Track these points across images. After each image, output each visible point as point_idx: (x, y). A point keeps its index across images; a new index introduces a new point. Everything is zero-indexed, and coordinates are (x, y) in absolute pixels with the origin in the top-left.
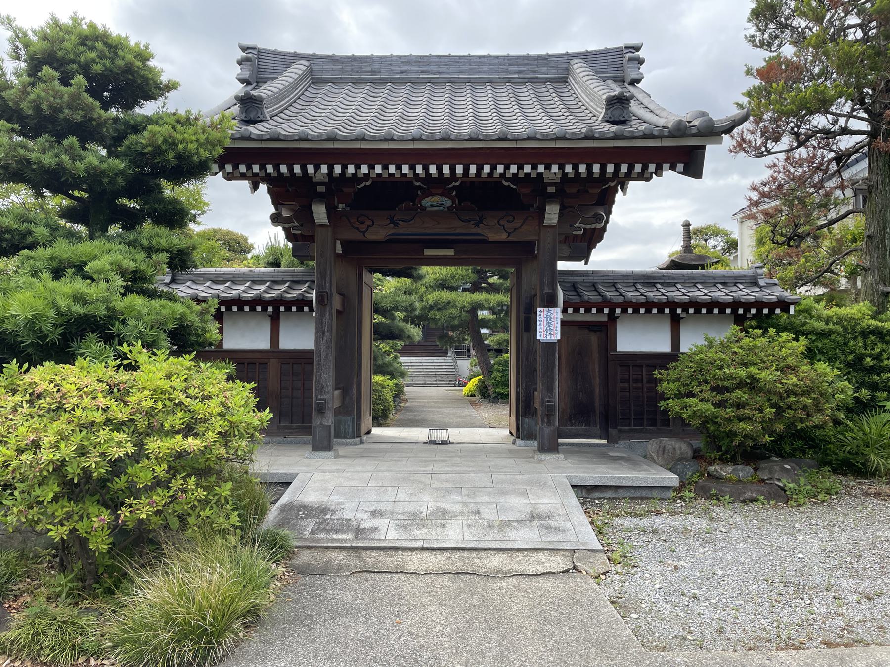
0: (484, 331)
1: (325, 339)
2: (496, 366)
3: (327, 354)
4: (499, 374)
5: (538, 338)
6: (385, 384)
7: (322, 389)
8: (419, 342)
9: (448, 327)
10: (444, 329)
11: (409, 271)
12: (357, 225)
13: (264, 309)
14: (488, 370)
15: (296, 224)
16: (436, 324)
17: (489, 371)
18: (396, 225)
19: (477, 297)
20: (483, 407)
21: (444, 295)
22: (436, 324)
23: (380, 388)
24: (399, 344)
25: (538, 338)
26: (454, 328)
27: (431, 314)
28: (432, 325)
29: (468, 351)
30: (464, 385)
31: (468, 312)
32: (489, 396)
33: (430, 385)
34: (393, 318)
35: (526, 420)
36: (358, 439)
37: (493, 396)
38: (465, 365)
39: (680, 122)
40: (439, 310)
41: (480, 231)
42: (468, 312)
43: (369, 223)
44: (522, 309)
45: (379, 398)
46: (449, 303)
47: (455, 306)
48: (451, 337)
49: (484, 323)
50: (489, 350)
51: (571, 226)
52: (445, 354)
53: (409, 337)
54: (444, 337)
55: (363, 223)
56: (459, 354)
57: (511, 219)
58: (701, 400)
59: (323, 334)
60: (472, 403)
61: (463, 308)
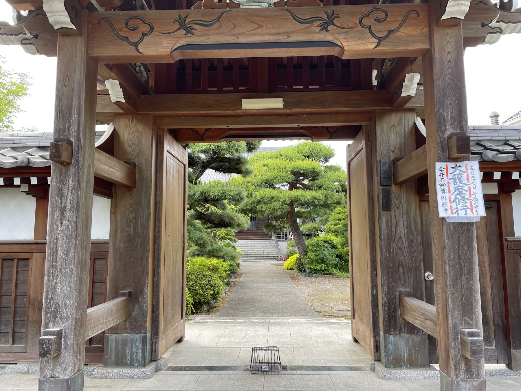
1: (66, 222)
2: (310, 247)
3: (68, 249)
4: (313, 254)
5: (442, 214)
6: (220, 265)
7: (56, 311)
8: (248, 229)
9: (272, 218)
10: (269, 219)
11: (238, 166)
12: (125, 32)
13: (25, 180)
14: (304, 251)
15: (28, 35)
16: (263, 215)
17: (305, 252)
18: (189, 30)
19: (296, 193)
20: (301, 281)
21: (269, 192)
22: (263, 215)
23: (210, 273)
24: (233, 231)
25: (442, 214)
26: (276, 218)
27: (259, 207)
28: (260, 216)
29: (286, 235)
30: (285, 259)
32: (305, 271)
33: (259, 260)
34: (224, 208)
35: (392, 338)
36: (153, 365)
38: (284, 245)
41: (329, 38)
43: (145, 28)
44: (376, 179)
45: (209, 283)
46: (273, 198)
47: (277, 200)
48: (274, 226)
49: (300, 215)
50: (303, 235)
51: (483, 25)
53: (239, 225)
54: (269, 226)
55: (134, 29)
56: (279, 237)
57: (382, 15)
58: (334, 247)
59: (63, 214)
60: (292, 277)
61: (283, 202)
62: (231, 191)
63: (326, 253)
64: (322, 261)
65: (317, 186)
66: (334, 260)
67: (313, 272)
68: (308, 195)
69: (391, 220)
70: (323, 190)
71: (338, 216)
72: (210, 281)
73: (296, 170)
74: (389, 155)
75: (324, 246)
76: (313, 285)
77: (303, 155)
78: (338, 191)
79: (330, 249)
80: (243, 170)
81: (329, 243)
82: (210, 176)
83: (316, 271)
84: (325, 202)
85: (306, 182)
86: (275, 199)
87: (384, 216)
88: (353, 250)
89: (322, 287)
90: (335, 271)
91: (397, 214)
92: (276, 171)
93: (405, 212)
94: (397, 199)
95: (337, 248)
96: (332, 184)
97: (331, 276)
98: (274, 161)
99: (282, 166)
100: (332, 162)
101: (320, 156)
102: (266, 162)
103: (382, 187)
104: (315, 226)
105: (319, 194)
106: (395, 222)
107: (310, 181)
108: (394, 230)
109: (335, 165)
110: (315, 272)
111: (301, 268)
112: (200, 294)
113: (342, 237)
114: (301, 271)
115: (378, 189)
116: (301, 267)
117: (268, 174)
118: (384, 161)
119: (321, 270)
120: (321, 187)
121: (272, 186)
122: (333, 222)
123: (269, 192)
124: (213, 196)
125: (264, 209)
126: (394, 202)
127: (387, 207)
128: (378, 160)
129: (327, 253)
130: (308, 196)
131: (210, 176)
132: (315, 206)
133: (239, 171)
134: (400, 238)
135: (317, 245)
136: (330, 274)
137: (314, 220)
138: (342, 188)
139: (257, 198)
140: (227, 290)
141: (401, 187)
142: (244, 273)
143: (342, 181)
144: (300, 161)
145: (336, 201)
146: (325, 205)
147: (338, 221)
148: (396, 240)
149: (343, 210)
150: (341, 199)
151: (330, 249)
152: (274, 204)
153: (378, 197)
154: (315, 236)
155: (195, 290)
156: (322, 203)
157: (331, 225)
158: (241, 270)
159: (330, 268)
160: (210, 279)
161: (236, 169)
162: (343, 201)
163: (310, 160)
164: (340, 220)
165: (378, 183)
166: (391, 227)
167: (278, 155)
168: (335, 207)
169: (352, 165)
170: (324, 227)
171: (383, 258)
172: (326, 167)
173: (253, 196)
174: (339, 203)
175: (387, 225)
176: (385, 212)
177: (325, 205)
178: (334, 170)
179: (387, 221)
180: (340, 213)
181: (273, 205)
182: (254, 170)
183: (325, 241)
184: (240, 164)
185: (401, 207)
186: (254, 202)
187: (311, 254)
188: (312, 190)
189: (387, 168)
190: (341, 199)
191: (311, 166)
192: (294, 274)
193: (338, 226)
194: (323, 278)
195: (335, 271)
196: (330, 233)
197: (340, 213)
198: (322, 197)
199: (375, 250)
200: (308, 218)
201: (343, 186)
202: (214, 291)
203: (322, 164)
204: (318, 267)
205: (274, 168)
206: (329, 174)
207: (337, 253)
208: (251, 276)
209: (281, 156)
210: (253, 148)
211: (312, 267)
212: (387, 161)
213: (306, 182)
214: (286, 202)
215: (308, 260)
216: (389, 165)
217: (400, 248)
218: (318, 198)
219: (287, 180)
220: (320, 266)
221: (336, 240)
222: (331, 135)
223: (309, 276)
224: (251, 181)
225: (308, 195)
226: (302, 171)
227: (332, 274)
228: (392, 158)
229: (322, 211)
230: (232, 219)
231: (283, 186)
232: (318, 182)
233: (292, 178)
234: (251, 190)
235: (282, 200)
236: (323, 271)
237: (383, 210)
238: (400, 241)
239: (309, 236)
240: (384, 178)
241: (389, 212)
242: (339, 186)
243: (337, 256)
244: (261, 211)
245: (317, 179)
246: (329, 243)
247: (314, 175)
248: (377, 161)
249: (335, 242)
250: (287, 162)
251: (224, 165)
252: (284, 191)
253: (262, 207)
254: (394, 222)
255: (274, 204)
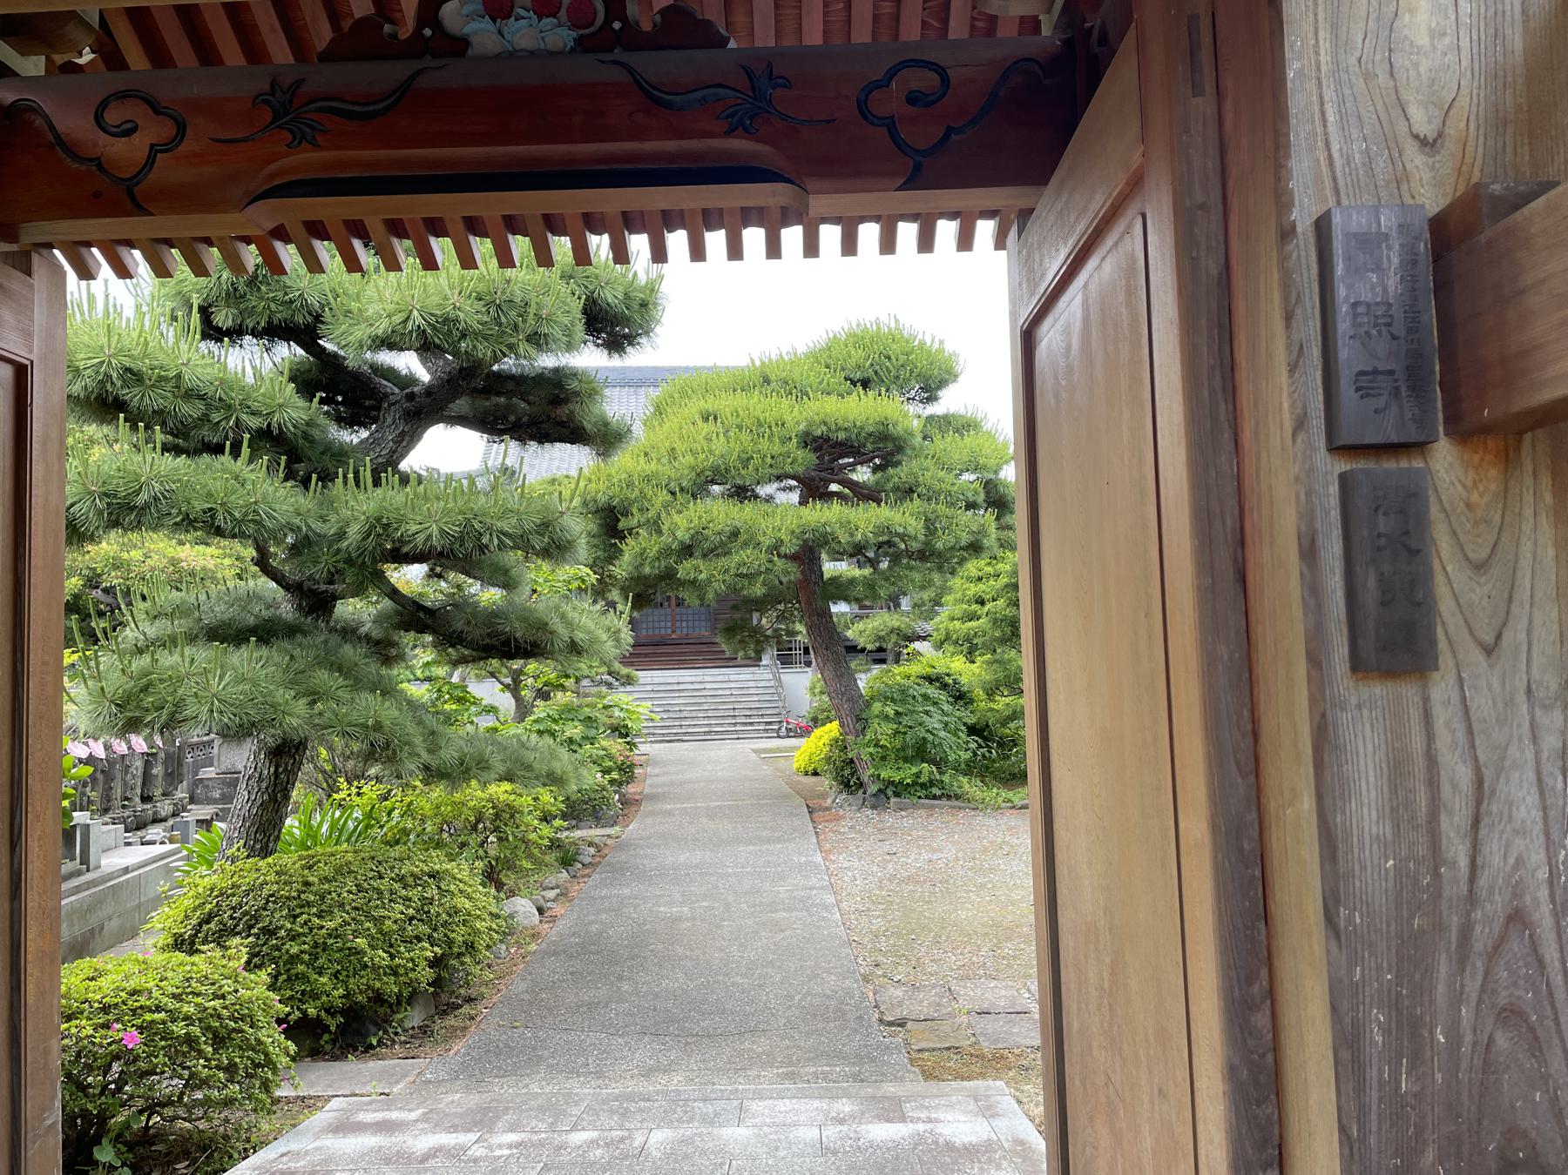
0: (839, 608)
2: (877, 707)
4: (889, 728)
11: (562, 412)
14: (856, 713)
17: (859, 719)
21: (718, 512)
27: (685, 569)
30: (805, 732)
31: (794, 557)
33: (721, 736)
37: (873, 789)
39: (314, 1060)
40: (710, 553)
42: (794, 557)
44: (1282, 393)
45: (423, 913)
46: (735, 534)
47: (752, 542)
49: (840, 589)
52: (756, 661)
56: (786, 660)
58: (961, 697)
61: (775, 548)
62: (506, 512)
63: (934, 722)
64: (920, 752)
65: (896, 489)
66: (960, 748)
67: (890, 793)
68: (866, 519)
69: (1431, 758)
70: (917, 502)
71: (974, 589)
72: (431, 901)
73: (819, 433)
74: (1401, 179)
75: (926, 697)
76: (886, 847)
77: (846, 379)
78: (971, 506)
79: (946, 707)
80: (588, 426)
81: (944, 686)
82: (556, 463)
83: (899, 789)
84: (927, 543)
85: (862, 475)
86: (742, 538)
87: (1368, 717)
88: (1059, 825)
89: (916, 859)
90: (967, 786)
91: (1482, 705)
92: (745, 437)
93: (1553, 682)
94: (1480, 567)
95: (972, 701)
96: (950, 478)
97: (955, 803)
98: (739, 400)
99: (769, 417)
100: (949, 401)
101: (907, 381)
102: (710, 405)
103: (1342, 466)
104: (896, 624)
105: (904, 518)
106: (1465, 775)
107: (876, 469)
108: (1459, 852)
109: (963, 412)
110: (890, 793)
111: (847, 776)
112: (376, 968)
113: (989, 663)
114: (847, 785)
115: (1295, 477)
116: (847, 772)
117: (719, 445)
118: (1359, 222)
119: (915, 783)
120: (911, 491)
121: (742, 493)
122: (959, 610)
123: (718, 512)
124: (421, 538)
125: (703, 576)
126: (1455, 590)
127: (1394, 637)
128: (1303, 217)
129: (939, 723)
130: (862, 525)
131: (556, 463)
132: (895, 559)
133: (575, 435)
134: (1518, 917)
135: (901, 695)
136: (949, 797)
137: (894, 602)
138: (987, 493)
139: (679, 534)
140: (551, 894)
141: (1508, 459)
142: (652, 797)
143: (985, 468)
144: (834, 398)
145: (965, 539)
146: (926, 554)
147: (975, 607)
148: (1482, 937)
149: (989, 569)
150: (982, 532)
151: (946, 707)
152: (743, 557)
153: (1309, 552)
154: (897, 661)
155: (359, 952)
156: (915, 546)
157: (953, 619)
158: (648, 781)
159: (946, 778)
160: (432, 892)
161: (562, 424)
162: (990, 541)
163: (870, 393)
164: (982, 603)
165: (1300, 424)
166: (1433, 818)
167: (758, 380)
168: (962, 562)
169: (1050, 337)
170: (929, 627)
171: (1363, 1110)
172: (930, 418)
173: (665, 528)
174: (975, 548)
175: (1397, 809)
176: (1378, 690)
177: (926, 554)
178: (957, 431)
179: (1397, 770)
180: (980, 579)
181: (736, 558)
182: (633, 428)
183: (930, 679)
184: (566, 401)
185: (1516, 634)
186: (666, 552)
187: (882, 731)
188: (878, 502)
189: (1393, 282)
190: (982, 532)
191: (876, 416)
192: (824, 796)
193: (973, 624)
194: (922, 812)
195: (967, 786)
196: (950, 648)
197: (980, 579)
198: (915, 527)
199: (1271, 993)
200: (865, 597)
201: (989, 486)
202: (450, 943)
203: (912, 408)
204: (906, 773)
205: (740, 427)
206: (939, 444)
207: (971, 720)
208: (669, 813)
209: (767, 381)
210: (625, 337)
211: (884, 774)
212: (1388, 220)
213: (862, 475)
214: (783, 550)
215: (871, 750)
216: (1410, 263)
217: (1510, 1015)
218: (901, 530)
219: (788, 469)
220: (915, 770)
221: (968, 672)
222: (918, 167)
223: (874, 807)
224: (655, 474)
225: (866, 519)
226: (842, 436)
227: (957, 797)
228: (1431, 198)
229: (917, 576)
230: (543, 626)
231: (784, 490)
232: (900, 474)
233: (804, 459)
234: (658, 505)
235: (767, 542)
236: (923, 786)
237: (1358, 665)
238: (1517, 946)
239: (879, 655)
240: (1367, 382)
241: (1408, 691)
242: (976, 485)
243: (973, 730)
244: (693, 582)
245: (897, 464)
246: (944, 686)
247: (885, 447)
248: (1287, 233)
249: (964, 680)
250: (785, 403)
251: (510, 408)
252: (784, 511)
253: (697, 569)
254: (1457, 771)
255: (743, 557)
